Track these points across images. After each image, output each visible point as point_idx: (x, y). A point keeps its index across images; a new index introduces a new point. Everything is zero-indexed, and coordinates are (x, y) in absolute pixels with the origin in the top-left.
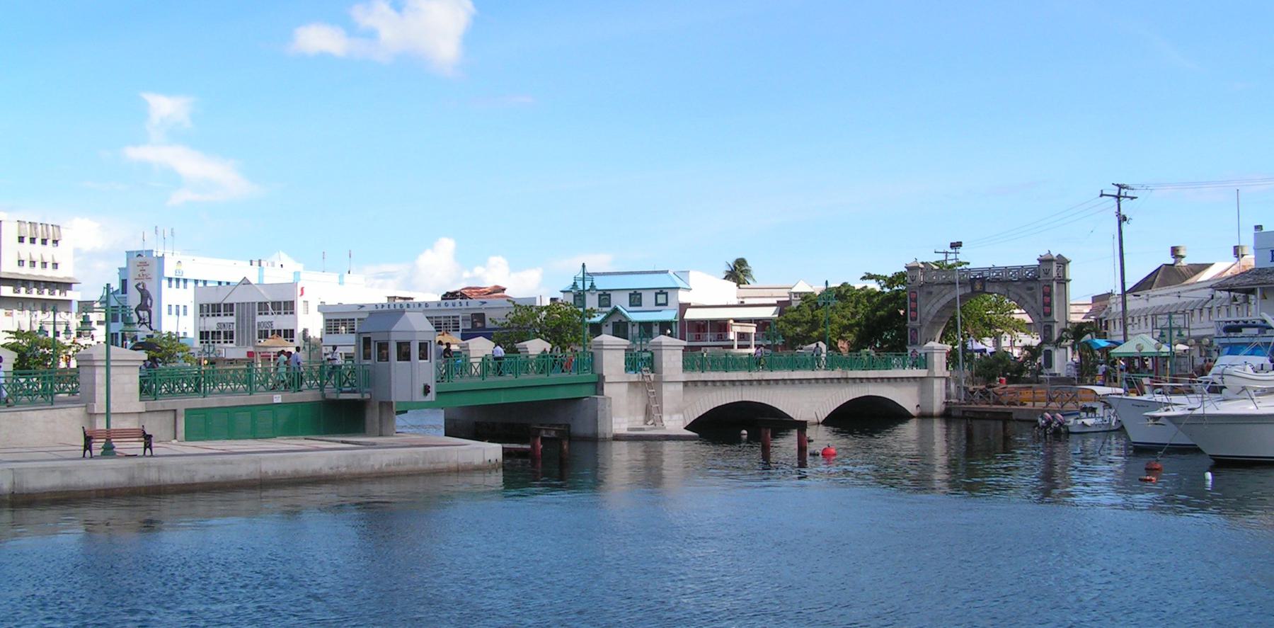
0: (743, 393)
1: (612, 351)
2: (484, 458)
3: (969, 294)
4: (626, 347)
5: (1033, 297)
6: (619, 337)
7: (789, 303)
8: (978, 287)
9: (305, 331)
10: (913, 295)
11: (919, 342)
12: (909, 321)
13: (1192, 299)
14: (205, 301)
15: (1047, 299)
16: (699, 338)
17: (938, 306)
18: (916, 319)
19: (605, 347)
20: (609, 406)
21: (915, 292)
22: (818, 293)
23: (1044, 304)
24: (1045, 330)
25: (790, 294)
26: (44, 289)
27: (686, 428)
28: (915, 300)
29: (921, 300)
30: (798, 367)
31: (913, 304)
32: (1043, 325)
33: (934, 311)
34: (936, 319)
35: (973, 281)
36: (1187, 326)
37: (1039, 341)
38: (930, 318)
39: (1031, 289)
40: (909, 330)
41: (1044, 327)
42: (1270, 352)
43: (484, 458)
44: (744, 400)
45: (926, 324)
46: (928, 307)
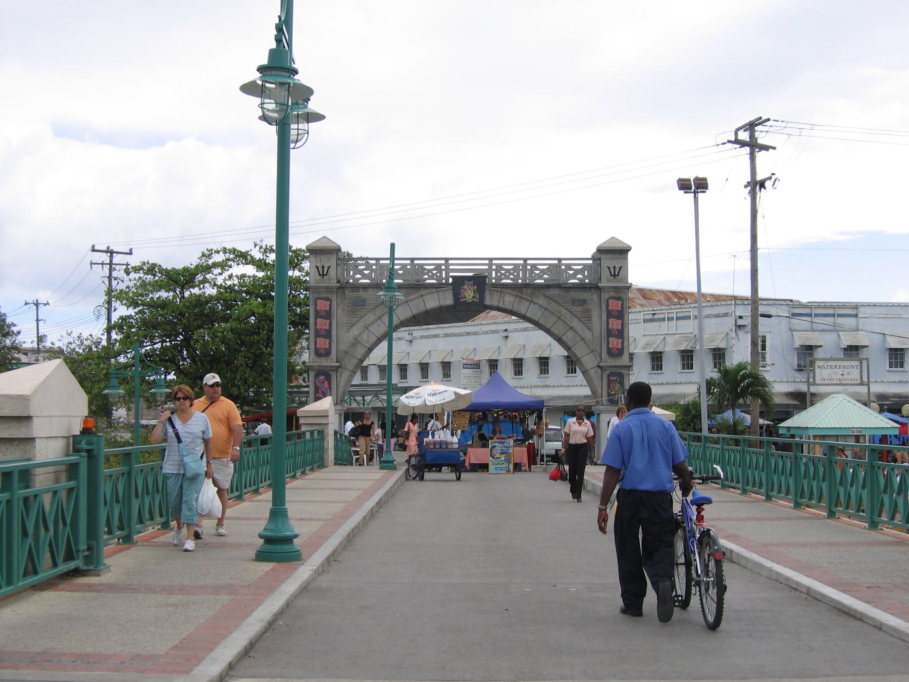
3: (448, 308)
5: (586, 318)
6: (859, 599)
8: (469, 294)
9: (207, 249)
10: (323, 305)
13: (484, 322)
14: (441, 376)
15: (615, 324)
16: (165, 439)
21: (327, 299)
22: (163, 290)
23: (610, 333)
24: (609, 382)
26: (651, 410)
28: (328, 315)
29: (339, 314)
30: (777, 574)
32: (608, 372)
35: (459, 282)
36: (865, 379)
39: (583, 302)
41: (608, 376)
42: (646, 407)
46: (356, 331)
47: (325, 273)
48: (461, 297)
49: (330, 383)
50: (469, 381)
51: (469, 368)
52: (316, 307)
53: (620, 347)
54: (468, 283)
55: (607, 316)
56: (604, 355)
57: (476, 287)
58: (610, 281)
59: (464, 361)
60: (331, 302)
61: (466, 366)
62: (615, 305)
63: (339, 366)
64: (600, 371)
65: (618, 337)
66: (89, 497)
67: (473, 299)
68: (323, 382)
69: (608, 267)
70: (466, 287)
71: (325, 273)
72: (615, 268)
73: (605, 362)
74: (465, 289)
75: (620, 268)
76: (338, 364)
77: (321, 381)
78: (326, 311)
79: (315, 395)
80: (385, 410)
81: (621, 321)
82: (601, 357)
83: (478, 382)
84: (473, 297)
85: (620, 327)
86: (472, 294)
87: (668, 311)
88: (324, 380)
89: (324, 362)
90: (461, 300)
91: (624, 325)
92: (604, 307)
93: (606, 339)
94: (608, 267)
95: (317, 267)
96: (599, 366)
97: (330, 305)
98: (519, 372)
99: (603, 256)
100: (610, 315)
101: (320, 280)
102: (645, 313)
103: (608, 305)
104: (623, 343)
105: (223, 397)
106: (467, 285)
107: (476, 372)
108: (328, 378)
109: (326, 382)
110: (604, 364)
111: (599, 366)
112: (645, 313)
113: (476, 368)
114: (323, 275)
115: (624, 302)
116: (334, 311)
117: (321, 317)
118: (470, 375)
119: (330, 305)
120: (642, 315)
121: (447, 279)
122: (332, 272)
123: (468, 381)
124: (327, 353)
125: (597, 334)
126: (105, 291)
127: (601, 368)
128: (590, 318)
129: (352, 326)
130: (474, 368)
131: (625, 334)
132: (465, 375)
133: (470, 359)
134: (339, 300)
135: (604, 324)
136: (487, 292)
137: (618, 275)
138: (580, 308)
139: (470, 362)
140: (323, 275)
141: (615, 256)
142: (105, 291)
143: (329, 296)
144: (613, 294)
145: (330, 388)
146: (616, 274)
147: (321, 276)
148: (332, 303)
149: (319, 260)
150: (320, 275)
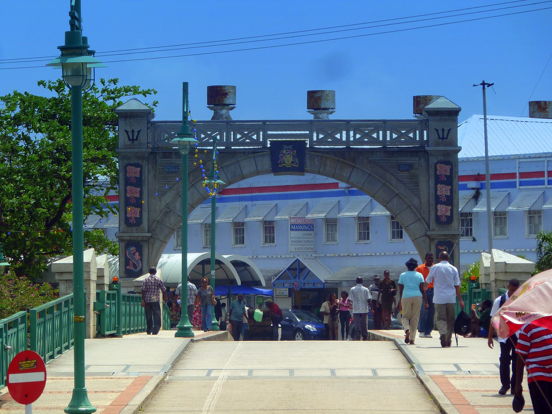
21: (137, 165)
23: (438, 200)
32: (436, 241)
39: (411, 166)
47: (135, 138)
48: (279, 162)
49: (141, 255)
50: (300, 247)
51: (299, 230)
52: (125, 174)
53: (449, 214)
54: (287, 147)
55: (435, 181)
56: (433, 224)
57: (295, 152)
58: (438, 145)
59: (293, 221)
60: (142, 169)
61: (295, 227)
62: (443, 170)
63: (151, 237)
64: (427, 240)
65: (446, 203)
66: (18, 336)
67: (293, 165)
68: (134, 254)
69: (436, 129)
70: (284, 152)
71: (135, 138)
72: (443, 130)
73: (434, 230)
74: (284, 154)
75: (449, 130)
76: (150, 235)
77: (132, 252)
78: (136, 178)
79: (126, 268)
80: (491, 183)
81: (450, 187)
82: (429, 226)
83: (312, 249)
84: (293, 162)
85: (449, 194)
86: (291, 160)
87: (548, 159)
88: (135, 251)
89: (136, 234)
90: (280, 166)
91: (454, 190)
92: (432, 173)
93: (434, 206)
94: (436, 129)
95: (127, 132)
96: (426, 235)
97: (141, 172)
98: (364, 235)
99: (431, 118)
100: (438, 180)
101: (130, 145)
102: (521, 160)
103: (436, 170)
104: (452, 211)
105: (418, 272)
106: (286, 149)
107: (309, 235)
108: (139, 249)
109: (137, 254)
110: (433, 233)
111: (426, 235)
112: (521, 160)
113: (308, 230)
114: (133, 140)
115: (454, 166)
116: (145, 178)
117: (131, 184)
118: (300, 240)
119: (141, 172)
120: (517, 163)
121: (265, 142)
122: (143, 138)
123: (297, 247)
124: (139, 222)
125: (424, 200)
126: (445, 343)
127: (429, 237)
128: (417, 184)
129: (163, 193)
130: (305, 230)
131: (455, 201)
132: (293, 239)
133: (300, 218)
134: (150, 166)
135: (432, 191)
136: (307, 156)
137: (447, 138)
138: (406, 174)
139: (300, 221)
140: (133, 140)
141: (443, 118)
142: (445, 343)
143: (140, 162)
144: (441, 158)
145: (141, 260)
146: (445, 136)
147: (131, 141)
148: (143, 170)
149: (128, 123)
150: (129, 139)
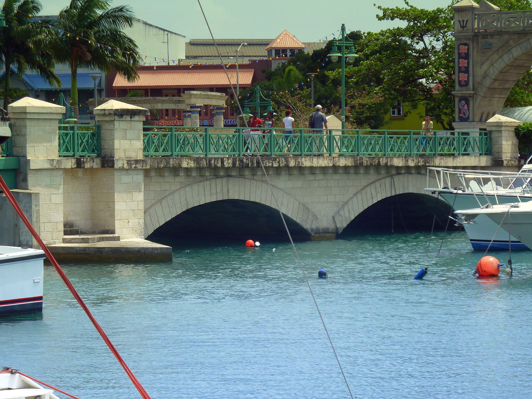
0: (230, 187)
1: (40, 123)
2: (370, 187)
4: (60, 117)
7: (268, 63)
11: (471, 119)
12: (457, 87)
17: (500, 65)
18: (467, 83)
19: (28, 116)
20: (36, 206)
21: (466, 44)
25: (270, 51)
27: (151, 238)
28: (466, 56)
29: (475, 56)
31: (463, 63)
33: (494, 72)
34: (496, 84)
37: (413, 165)
38: (488, 82)
40: (457, 100)
43: (370, 187)
44: (231, 198)
45: (482, 92)
46: (485, 67)
